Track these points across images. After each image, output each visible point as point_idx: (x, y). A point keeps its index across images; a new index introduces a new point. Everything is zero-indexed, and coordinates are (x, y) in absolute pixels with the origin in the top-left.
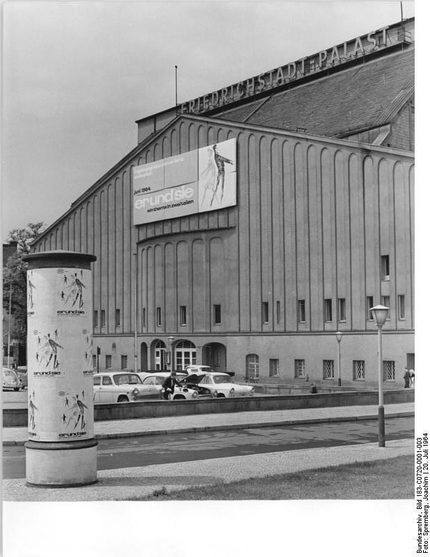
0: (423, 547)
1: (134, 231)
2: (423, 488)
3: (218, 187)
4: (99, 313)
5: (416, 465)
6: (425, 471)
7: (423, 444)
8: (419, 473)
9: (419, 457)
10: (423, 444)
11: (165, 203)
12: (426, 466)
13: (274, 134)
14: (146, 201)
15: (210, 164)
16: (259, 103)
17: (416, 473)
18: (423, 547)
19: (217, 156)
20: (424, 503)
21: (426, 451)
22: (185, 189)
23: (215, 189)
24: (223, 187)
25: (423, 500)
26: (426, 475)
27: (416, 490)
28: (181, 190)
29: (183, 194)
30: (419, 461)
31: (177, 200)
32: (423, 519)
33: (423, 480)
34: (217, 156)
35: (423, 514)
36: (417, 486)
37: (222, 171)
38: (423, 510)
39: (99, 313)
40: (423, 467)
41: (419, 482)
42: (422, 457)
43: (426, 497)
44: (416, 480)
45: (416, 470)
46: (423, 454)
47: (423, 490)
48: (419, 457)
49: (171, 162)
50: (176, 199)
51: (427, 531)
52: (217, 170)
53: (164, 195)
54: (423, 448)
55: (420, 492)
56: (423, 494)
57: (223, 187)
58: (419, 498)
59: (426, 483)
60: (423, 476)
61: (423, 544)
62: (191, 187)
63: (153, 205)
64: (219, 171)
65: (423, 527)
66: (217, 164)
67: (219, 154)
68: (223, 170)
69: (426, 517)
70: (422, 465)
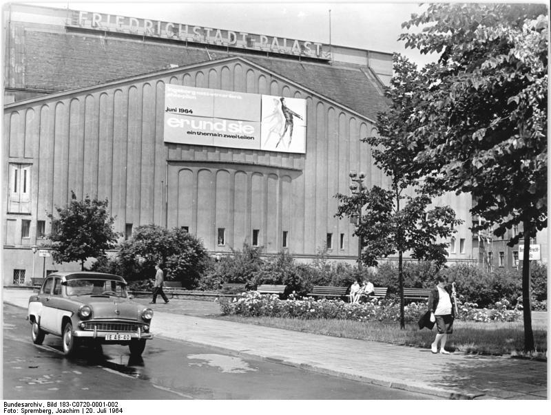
0: (10, 408)
1: (161, 149)
2: (68, 408)
3: (286, 133)
4: (33, 225)
5: (91, 402)
6: (85, 411)
7: (112, 408)
8: (83, 404)
9: (99, 404)
10: (112, 408)
11: (214, 130)
12: (90, 411)
13: (342, 109)
14: (185, 123)
15: (276, 112)
16: (235, 56)
17: (83, 401)
18: (10, 408)
19: (284, 108)
20: (54, 409)
21: (105, 411)
22: (243, 125)
23: (282, 134)
24: (291, 135)
25: (57, 407)
26: (81, 411)
27: (66, 401)
28: (238, 124)
29: (240, 129)
30: (95, 405)
31: (232, 133)
32: (38, 408)
33: (76, 408)
34: (284, 108)
35: (42, 408)
36: (71, 402)
37: (290, 122)
38: (46, 408)
39: (33, 225)
40: (89, 408)
41: (74, 404)
42: (99, 407)
43: (59, 411)
44: (76, 401)
45: (86, 401)
46: (102, 408)
47: (66, 408)
48: (99, 405)
49: (224, 96)
50: (231, 131)
51: (25, 412)
52: (284, 119)
53: (214, 123)
54: (108, 408)
55: (64, 405)
56: (62, 408)
57: (291, 135)
58: (58, 405)
59: (74, 411)
60: (80, 408)
61: (13, 408)
62: (254, 126)
63: (194, 128)
64: (287, 121)
65: (29, 408)
66: (285, 115)
67: (287, 106)
68: (291, 121)
69: (40, 411)
70: (91, 407)
